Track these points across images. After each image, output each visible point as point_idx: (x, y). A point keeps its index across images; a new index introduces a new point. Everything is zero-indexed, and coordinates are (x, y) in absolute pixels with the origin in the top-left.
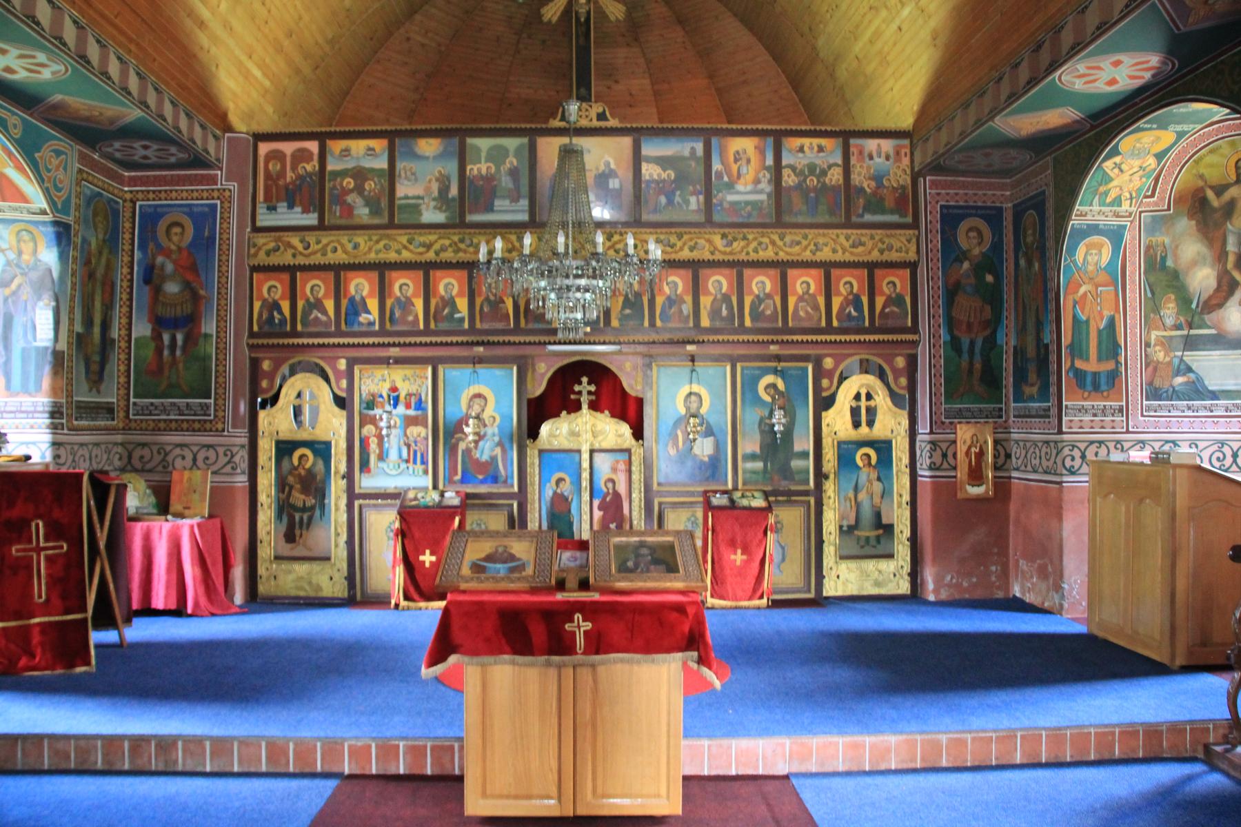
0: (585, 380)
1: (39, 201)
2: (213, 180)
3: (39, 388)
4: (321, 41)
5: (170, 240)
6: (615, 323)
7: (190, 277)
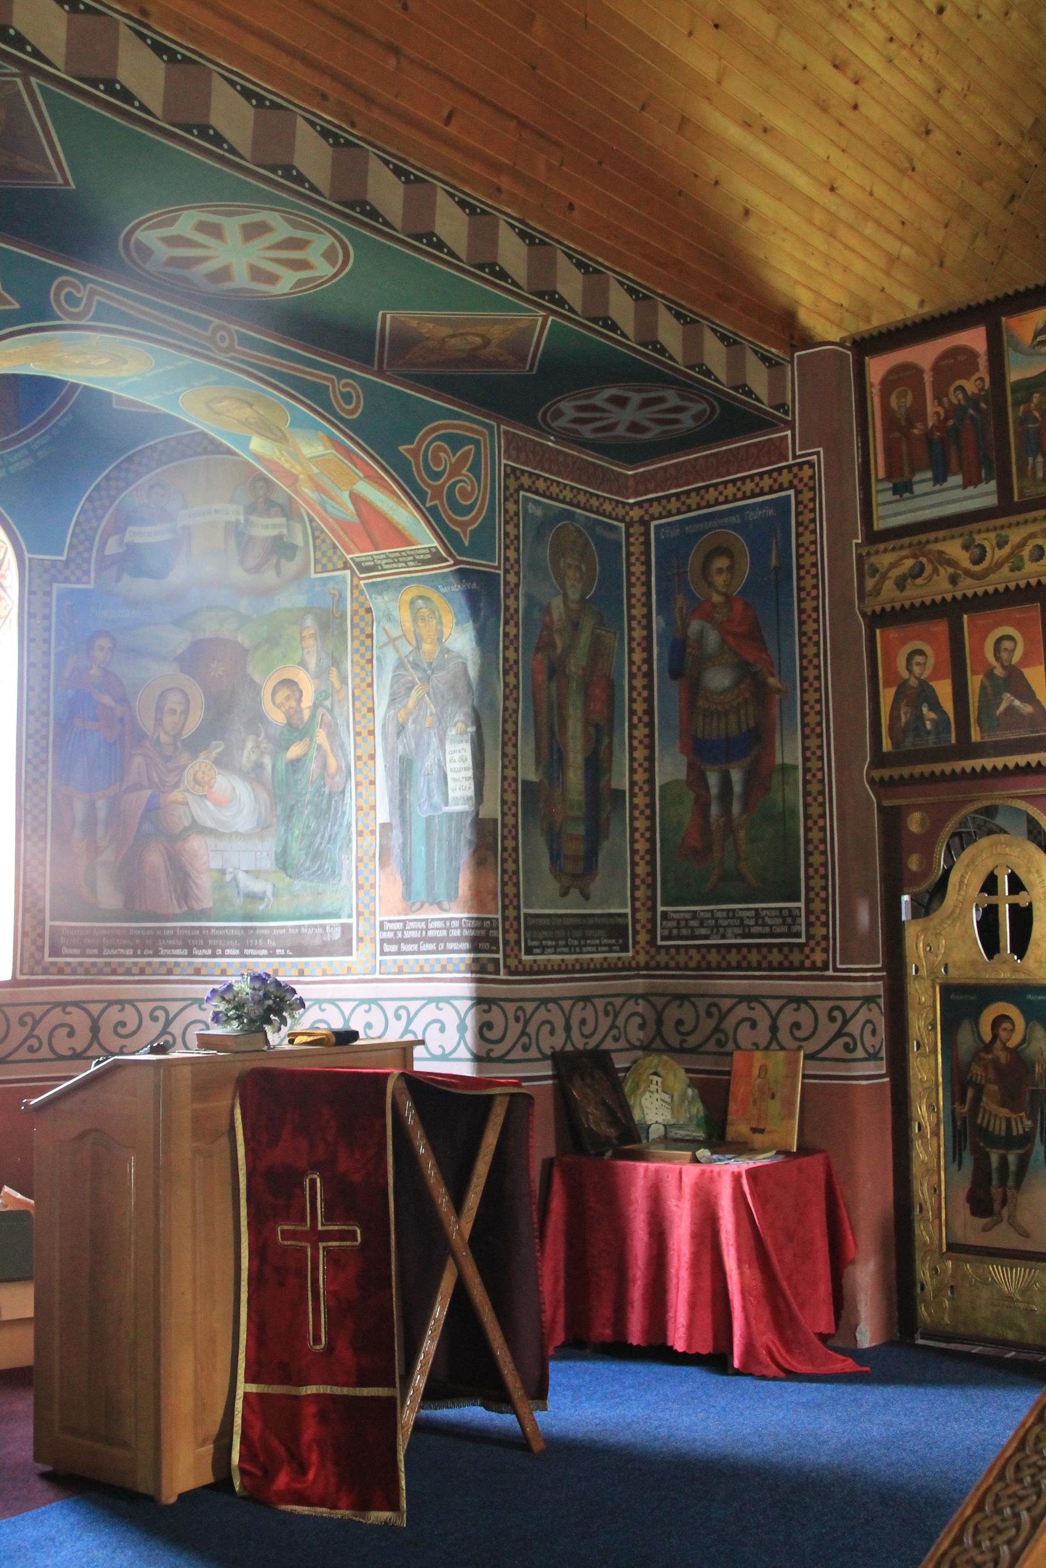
1: (427, 540)
3: (452, 896)
4: (1007, 134)
5: (711, 585)
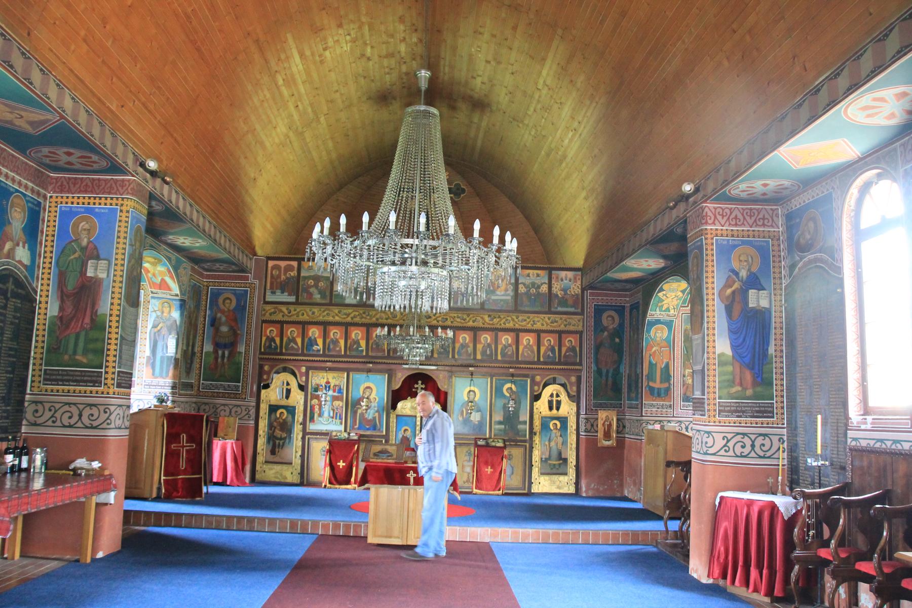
0: (420, 382)
1: (175, 289)
2: (247, 278)
6: (436, 355)
7: (233, 324)
